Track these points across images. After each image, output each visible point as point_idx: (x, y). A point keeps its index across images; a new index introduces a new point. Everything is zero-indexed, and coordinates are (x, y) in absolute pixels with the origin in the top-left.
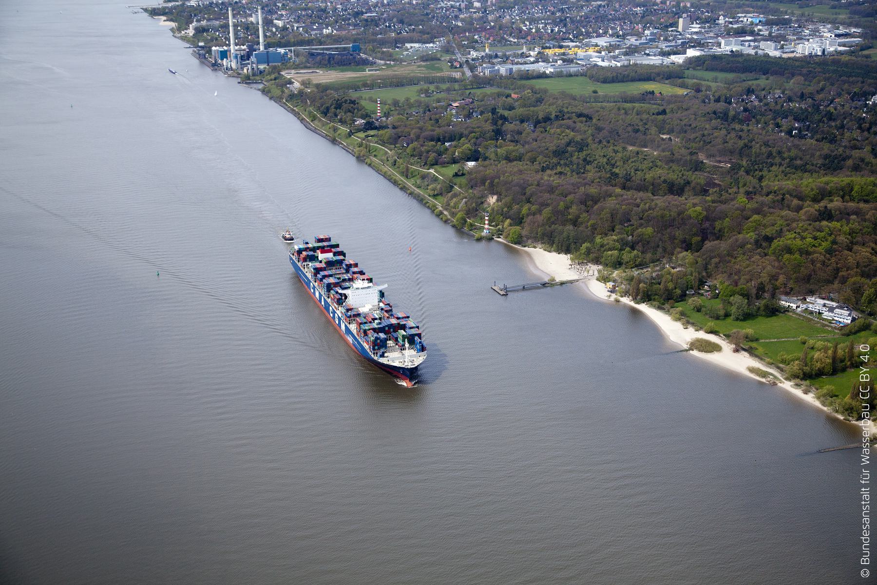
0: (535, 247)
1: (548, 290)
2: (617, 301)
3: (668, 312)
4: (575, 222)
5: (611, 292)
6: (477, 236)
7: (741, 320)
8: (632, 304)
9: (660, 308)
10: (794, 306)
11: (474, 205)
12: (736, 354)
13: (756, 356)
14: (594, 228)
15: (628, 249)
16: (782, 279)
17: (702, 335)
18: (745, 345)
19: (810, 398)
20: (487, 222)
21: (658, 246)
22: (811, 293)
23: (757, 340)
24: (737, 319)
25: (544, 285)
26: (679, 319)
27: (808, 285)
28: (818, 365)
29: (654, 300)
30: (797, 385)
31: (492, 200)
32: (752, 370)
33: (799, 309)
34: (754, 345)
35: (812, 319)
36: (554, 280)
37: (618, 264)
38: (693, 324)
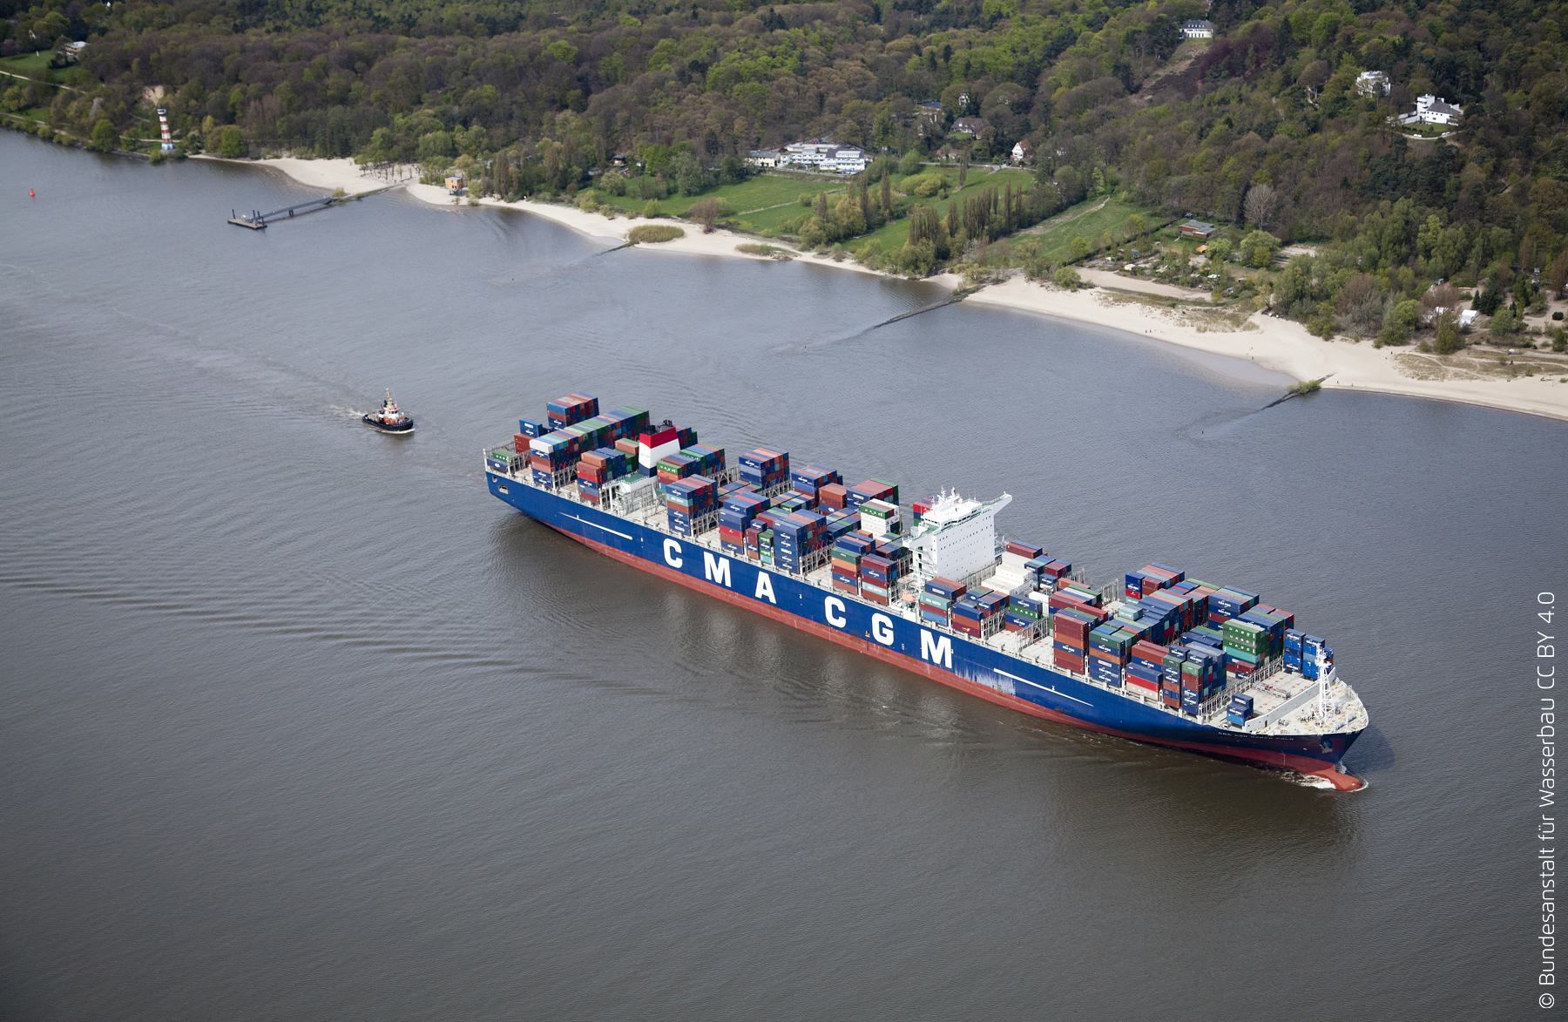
0: (278, 157)
1: (337, 210)
2: (474, 205)
3: (570, 203)
4: (343, 99)
5: (456, 193)
6: (152, 155)
7: (696, 194)
8: (503, 204)
9: (555, 200)
10: (771, 162)
11: (122, 105)
12: (710, 236)
13: (743, 232)
14: (383, 102)
15: (458, 127)
16: (739, 124)
17: (641, 222)
18: (715, 221)
19: (848, 265)
20: (164, 127)
21: (511, 117)
22: (791, 139)
23: (733, 214)
24: (689, 193)
25: (329, 203)
26: (597, 210)
27: (786, 126)
28: (845, 221)
29: (540, 191)
30: (823, 254)
31: (156, 94)
32: (744, 249)
33: (780, 165)
34: (732, 220)
35: (801, 175)
36: (343, 194)
37: (452, 152)
38: (622, 212)
